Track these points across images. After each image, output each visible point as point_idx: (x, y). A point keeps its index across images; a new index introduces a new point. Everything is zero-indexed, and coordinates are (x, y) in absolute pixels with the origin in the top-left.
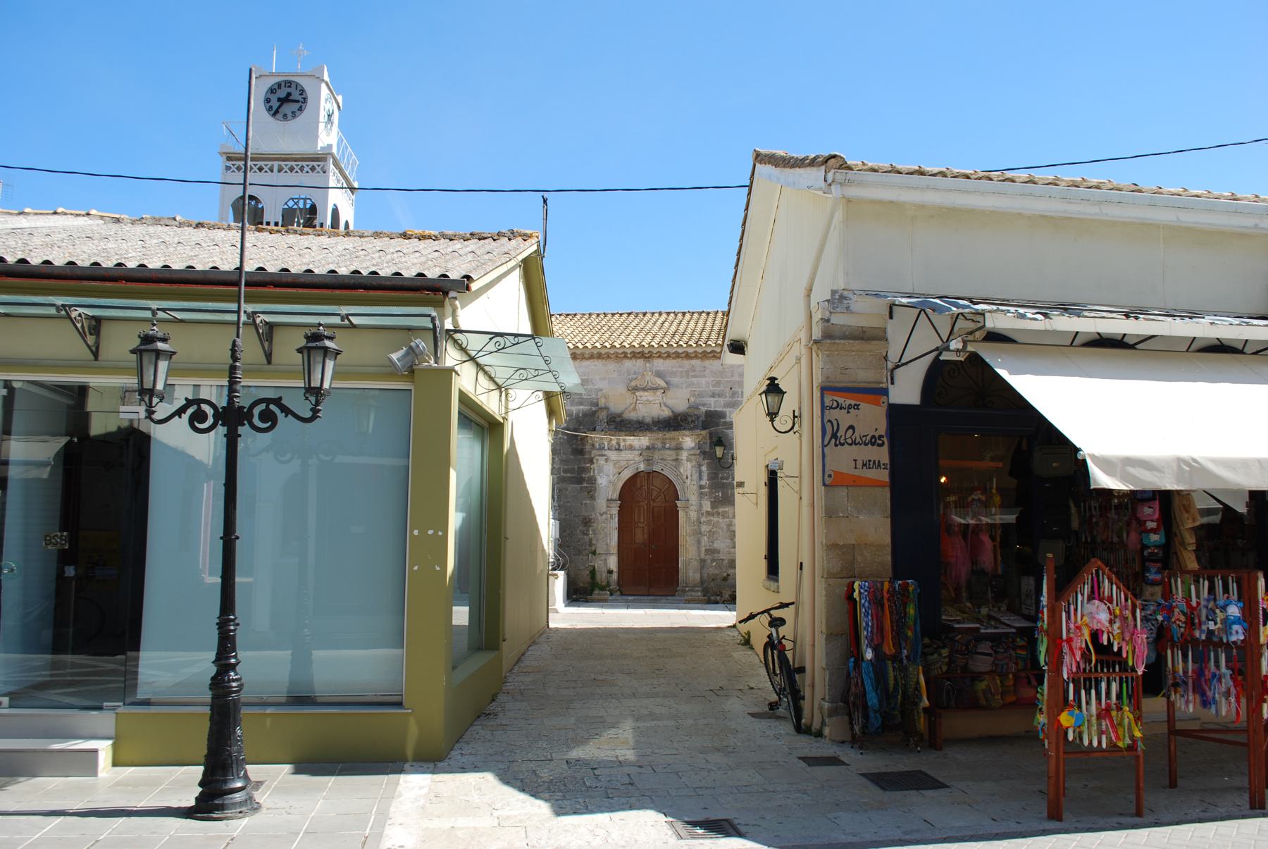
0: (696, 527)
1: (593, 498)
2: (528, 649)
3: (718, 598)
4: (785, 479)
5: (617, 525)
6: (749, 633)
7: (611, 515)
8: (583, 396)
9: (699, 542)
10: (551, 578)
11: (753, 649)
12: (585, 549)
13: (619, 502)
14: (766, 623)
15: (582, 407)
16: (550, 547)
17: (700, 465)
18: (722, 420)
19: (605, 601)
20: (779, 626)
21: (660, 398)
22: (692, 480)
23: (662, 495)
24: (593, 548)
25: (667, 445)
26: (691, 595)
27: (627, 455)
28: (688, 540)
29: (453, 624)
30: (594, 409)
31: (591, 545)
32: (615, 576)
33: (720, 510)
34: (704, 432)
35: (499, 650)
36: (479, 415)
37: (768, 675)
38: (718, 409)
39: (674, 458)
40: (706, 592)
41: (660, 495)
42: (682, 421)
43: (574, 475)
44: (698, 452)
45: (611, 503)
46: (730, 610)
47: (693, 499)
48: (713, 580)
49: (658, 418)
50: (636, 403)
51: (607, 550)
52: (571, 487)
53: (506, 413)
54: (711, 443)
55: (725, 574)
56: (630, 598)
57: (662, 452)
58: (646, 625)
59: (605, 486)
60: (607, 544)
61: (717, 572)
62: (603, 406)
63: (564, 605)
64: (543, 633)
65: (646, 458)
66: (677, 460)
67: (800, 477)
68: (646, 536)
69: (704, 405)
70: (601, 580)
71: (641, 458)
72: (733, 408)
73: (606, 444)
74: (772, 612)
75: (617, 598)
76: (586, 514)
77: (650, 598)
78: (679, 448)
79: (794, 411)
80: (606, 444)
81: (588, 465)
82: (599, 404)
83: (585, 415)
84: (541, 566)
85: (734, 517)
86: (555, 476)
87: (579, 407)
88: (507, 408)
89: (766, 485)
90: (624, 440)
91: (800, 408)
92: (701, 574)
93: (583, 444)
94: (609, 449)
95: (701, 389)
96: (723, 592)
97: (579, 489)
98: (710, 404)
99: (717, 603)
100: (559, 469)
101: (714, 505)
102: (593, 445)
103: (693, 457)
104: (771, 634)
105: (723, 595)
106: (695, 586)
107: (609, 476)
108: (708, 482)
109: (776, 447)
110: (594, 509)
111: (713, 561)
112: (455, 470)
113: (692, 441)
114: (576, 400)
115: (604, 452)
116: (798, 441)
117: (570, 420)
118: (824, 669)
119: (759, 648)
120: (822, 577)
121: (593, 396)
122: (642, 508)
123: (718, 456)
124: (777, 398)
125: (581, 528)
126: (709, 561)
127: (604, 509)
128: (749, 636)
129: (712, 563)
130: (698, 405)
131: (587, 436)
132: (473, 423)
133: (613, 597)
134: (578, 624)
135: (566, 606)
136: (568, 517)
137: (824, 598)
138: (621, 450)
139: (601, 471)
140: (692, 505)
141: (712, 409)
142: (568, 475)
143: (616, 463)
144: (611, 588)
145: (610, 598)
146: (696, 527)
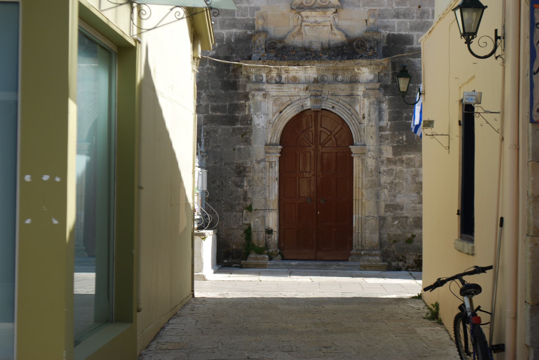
0: (374, 178)
1: (248, 142)
2: (168, 323)
3: (401, 264)
4: (484, 115)
5: (277, 175)
6: (437, 305)
7: (271, 163)
8: (236, 17)
9: (378, 196)
10: (197, 239)
11: (442, 324)
12: (239, 204)
13: (280, 147)
14: (457, 291)
15: (234, 30)
16: (196, 201)
17: (380, 102)
18: (408, 46)
19: (263, 266)
20: (473, 295)
21: (331, 19)
22: (369, 120)
23: (333, 139)
24: (248, 203)
25: (340, 78)
26: (368, 260)
27: (289, 90)
28: (364, 193)
29: (75, 293)
30: (249, 32)
31: (245, 199)
32: (275, 237)
33: (405, 157)
34: (385, 61)
35: (132, 322)
36: (103, 34)
37: (460, 354)
38: (403, 33)
39: (348, 93)
40: (385, 256)
41: (331, 139)
42: (358, 48)
43: (224, 114)
44: (377, 85)
45: (270, 149)
46: (415, 278)
47: (371, 143)
48: (395, 242)
49: (329, 44)
50: (301, 25)
51: (266, 204)
52: (221, 129)
53: (139, 34)
54: (394, 74)
55: (409, 236)
56: (294, 263)
57: (333, 86)
58: (311, 295)
59: (263, 127)
60: (265, 199)
61: (399, 232)
62: (260, 28)
63: (212, 271)
64: (187, 304)
65: (313, 93)
66: (351, 95)
67: (502, 113)
68: (313, 189)
69: (385, 27)
70: (258, 240)
71: (308, 93)
72: (421, 31)
73: (264, 75)
74: (465, 278)
75: (278, 263)
76: (240, 161)
77: (318, 263)
78: (354, 81)
79: (496, 31)
80: (264, 75)
81: (242, 102)
82: (256, 26)
83: (239, 40)
84: (184, 222)
85: (421, 166)
86: (201, 115)
87: (231, 31)
88: (139, 28)
89: (460, 124)
90: (287, 72)
91: (504, 27)
92: (380, 234)
93: (237, 77)
94: (268, 82)
95: (382, 8)
96: (407, 256)
97: (231, 130)
98: (394, 27)
99: (399, 269)
100: (207, 106)
101: (397, 151)
102: (248, 77)
103: (371, 93)
104: (464, 304)
105: (407, 261)
106: (373, 249)
107: (268, 115)
108: (389, 123)
109: (473, 77)
110: (249, 155)
111: (395, 218)
112: (75, 101)
113: (370, 72)
114: (227, 22)
115: (261, 86)
116: (501, 68)
117: (220, 46)
118: (528, 346)
119: (449, 323)
120: (528, 235)
121: (249, 17)
122: (308, 154)
123: (402, 90)
124: (475, 14)
125: (233, 178)
126: (390, 219)
127: (261, 156)
128: (438, 309)
129: (393, 221)
130: (379, 27)
131: (241, 66)
132: (98, 47)
133: (272, 262)
134: (230, 293)
135: (215, 273)
136: (218, 165)
137: (528, 261)
138: (283, 83)
139: (258, 109)
140: (369, 151)
141: (396, 33)
142: (218, 114)
143: (276, 99)
144: (270, 251)
145: (269, 263)
146: (374, 178)
